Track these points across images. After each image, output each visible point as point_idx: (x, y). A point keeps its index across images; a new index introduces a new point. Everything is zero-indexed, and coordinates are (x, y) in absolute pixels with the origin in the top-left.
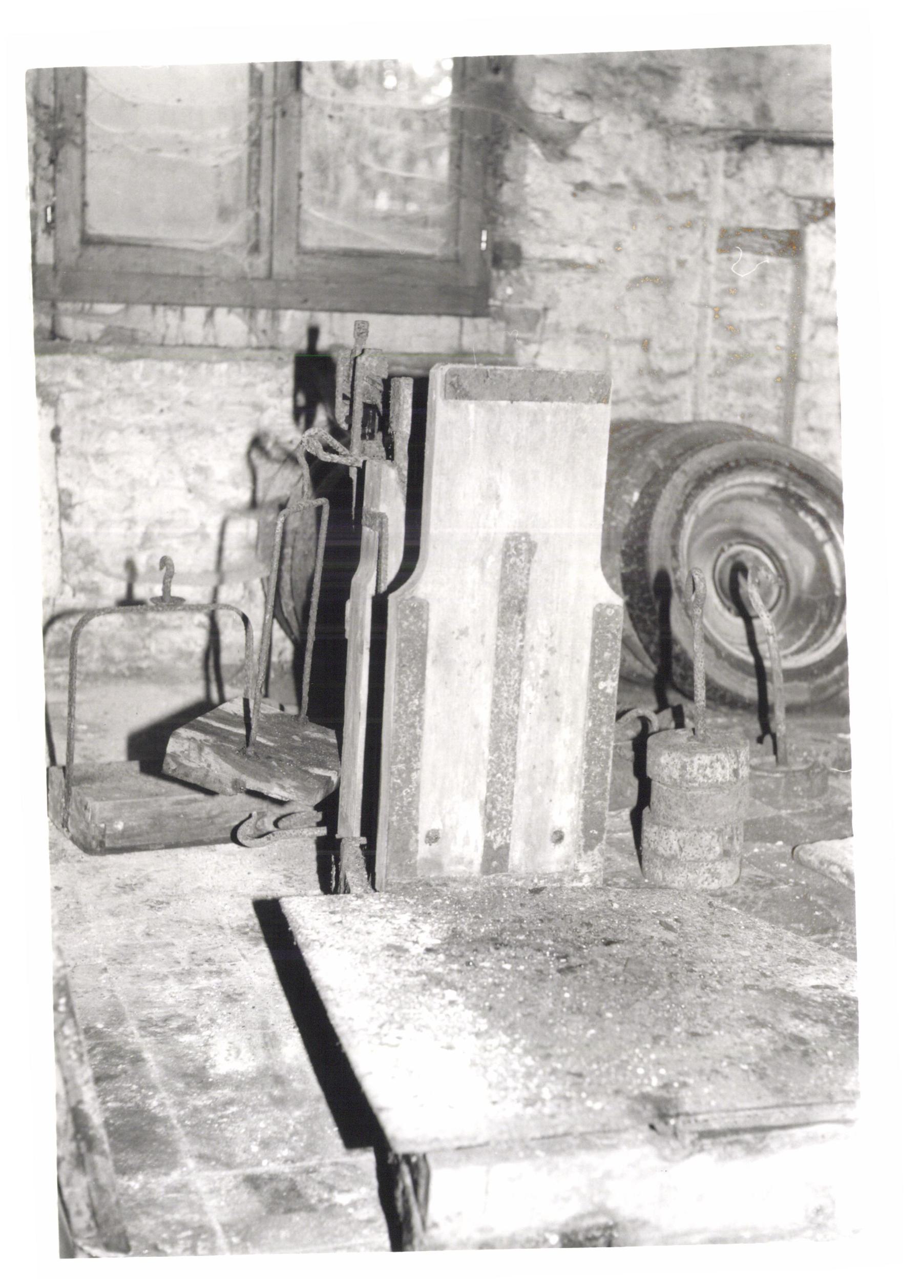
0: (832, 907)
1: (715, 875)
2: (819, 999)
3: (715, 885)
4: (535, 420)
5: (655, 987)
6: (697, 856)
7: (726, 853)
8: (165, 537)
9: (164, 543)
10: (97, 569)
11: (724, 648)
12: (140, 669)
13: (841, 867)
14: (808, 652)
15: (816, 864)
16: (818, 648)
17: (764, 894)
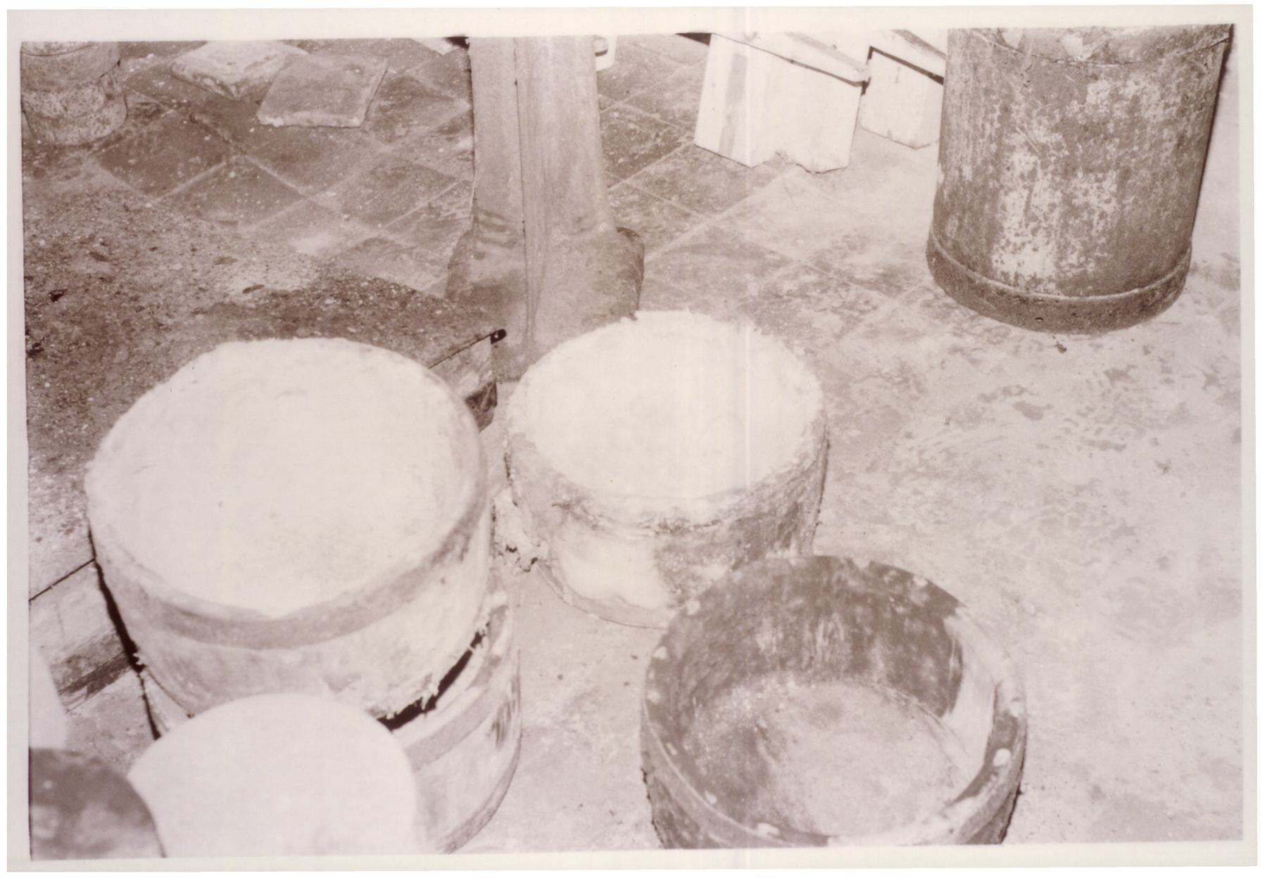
1: (105, 122)
2: (252, 305)
3: (107, 131)
4: (1182, 305)
5: (116, 345)
6: (83, 111)
7: (109, 97)
13: (214, 79)
15: (190, 78)
17: (155, 126)
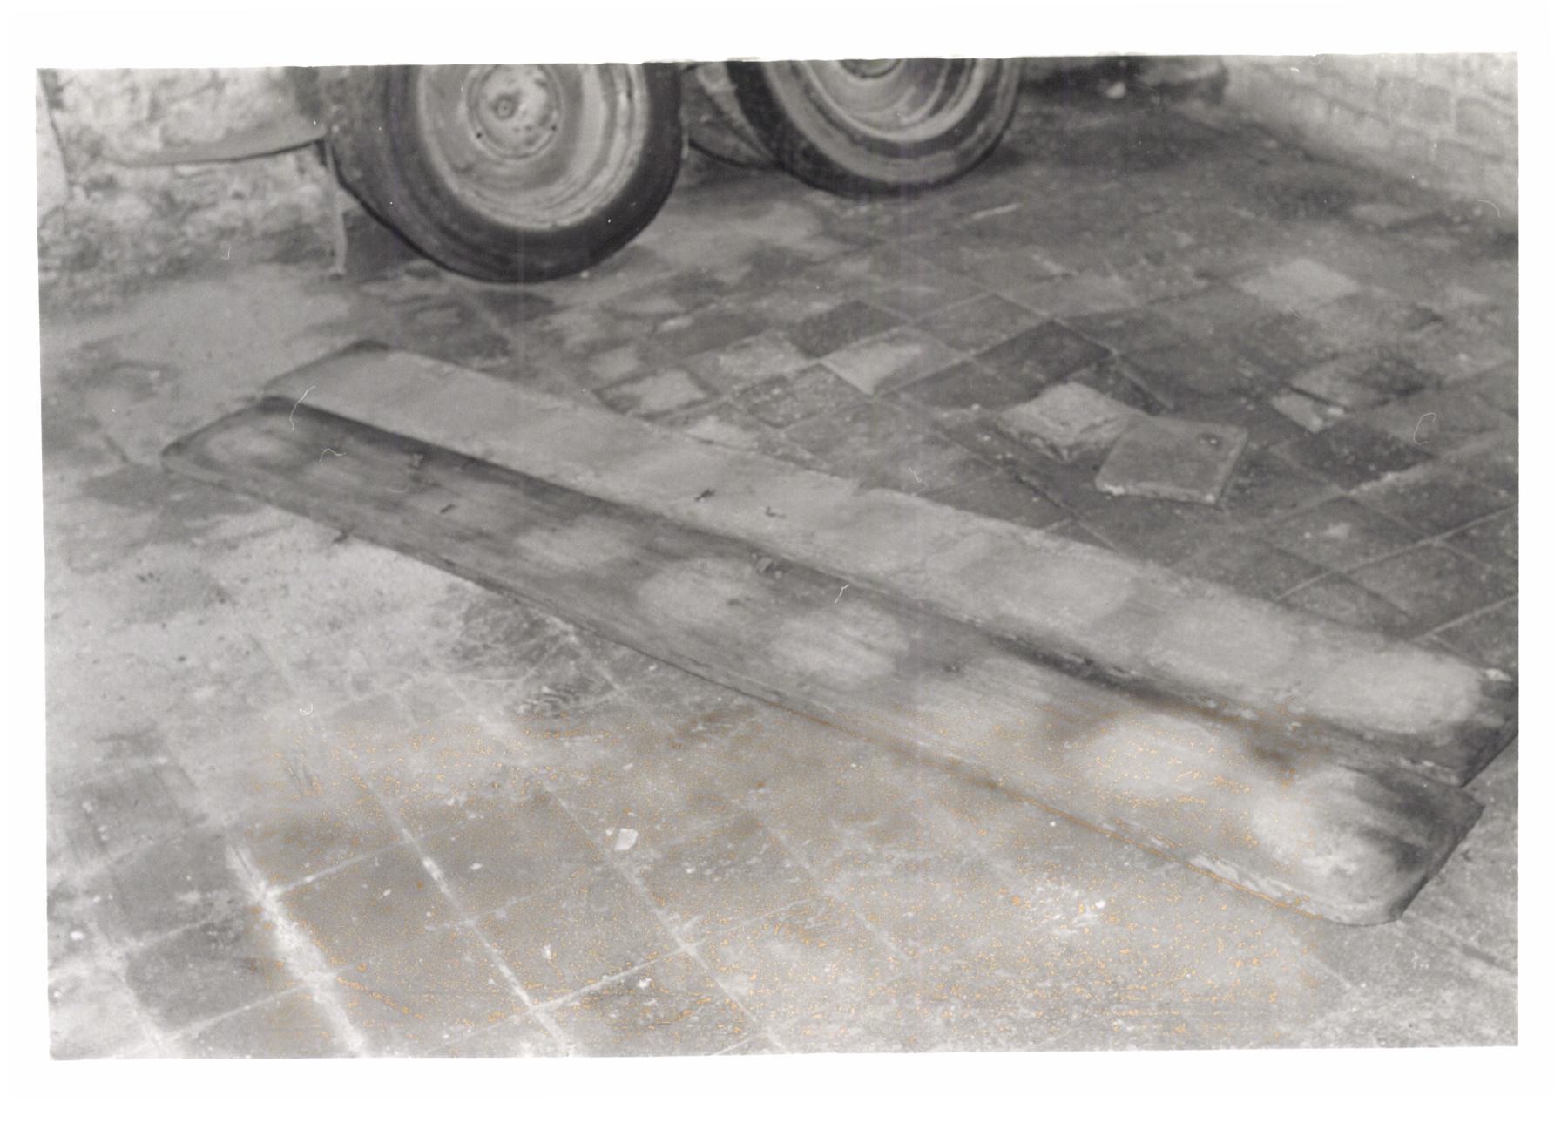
0: (1046, 487)
8: (174, 100)
9: (175, 108)
10: (106, 159)
11: (856, 130)
12: (181, 261)
13: (1043, 439)
14: (946, 108)
16: (956, 104)
